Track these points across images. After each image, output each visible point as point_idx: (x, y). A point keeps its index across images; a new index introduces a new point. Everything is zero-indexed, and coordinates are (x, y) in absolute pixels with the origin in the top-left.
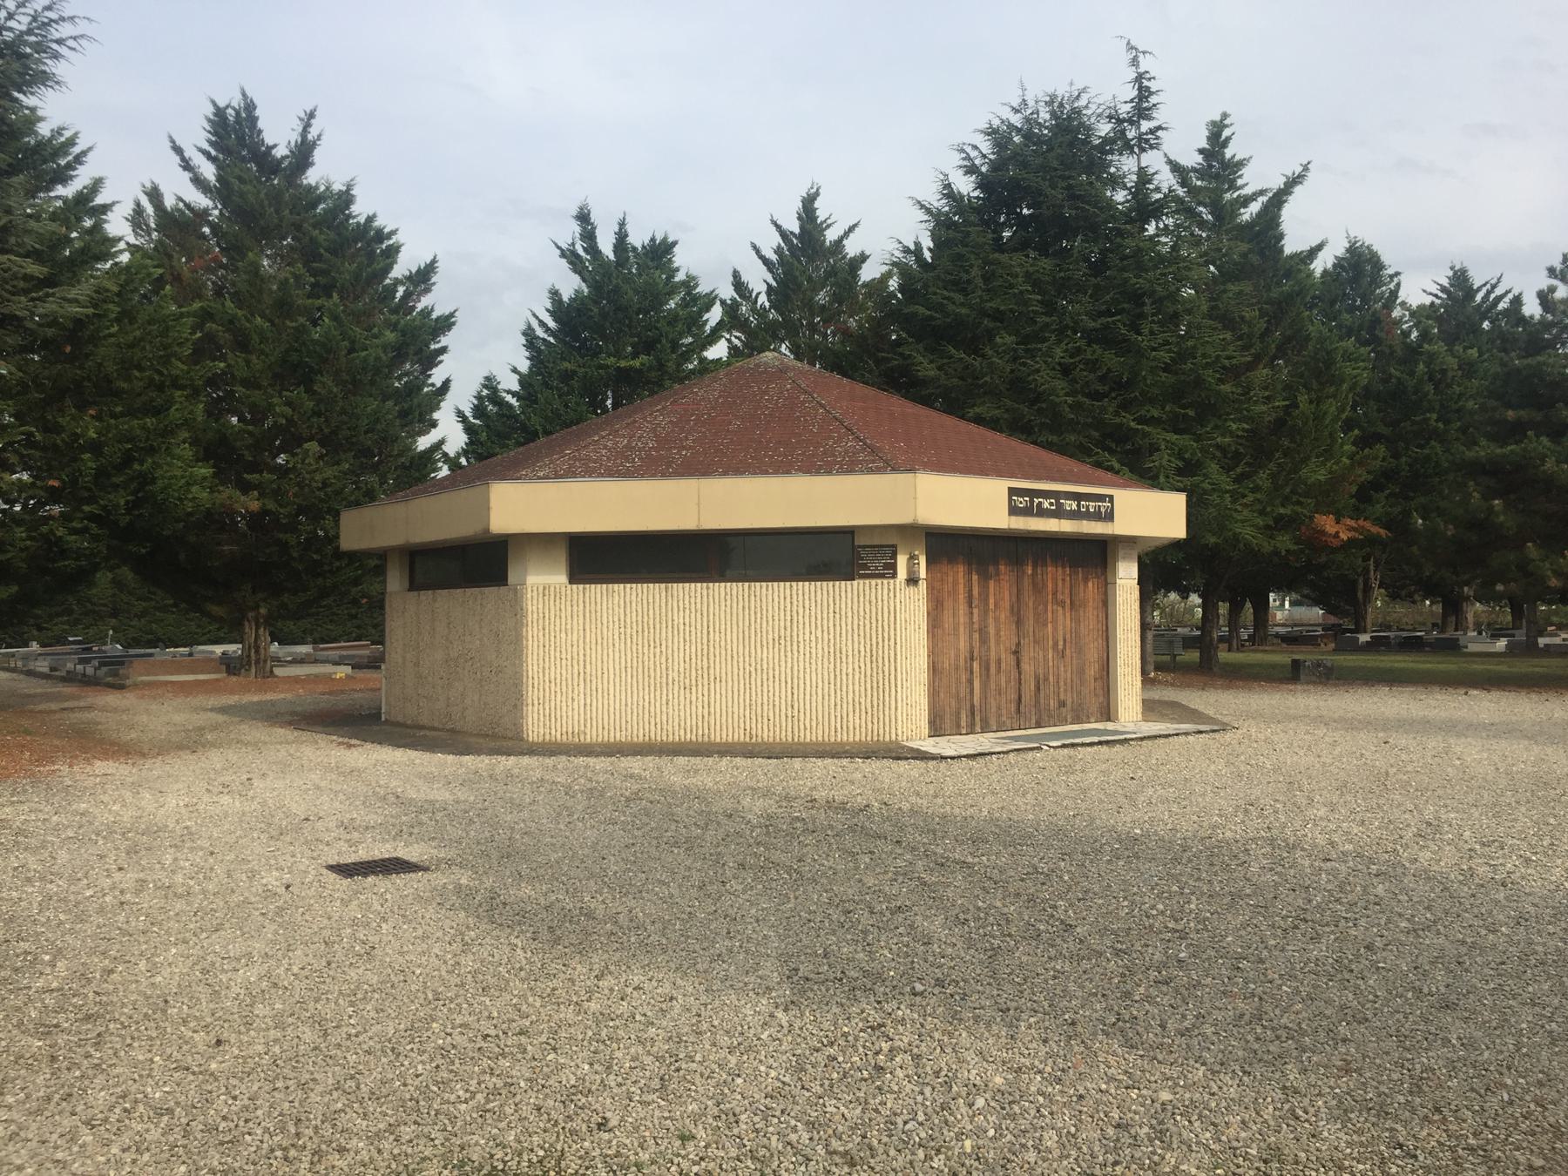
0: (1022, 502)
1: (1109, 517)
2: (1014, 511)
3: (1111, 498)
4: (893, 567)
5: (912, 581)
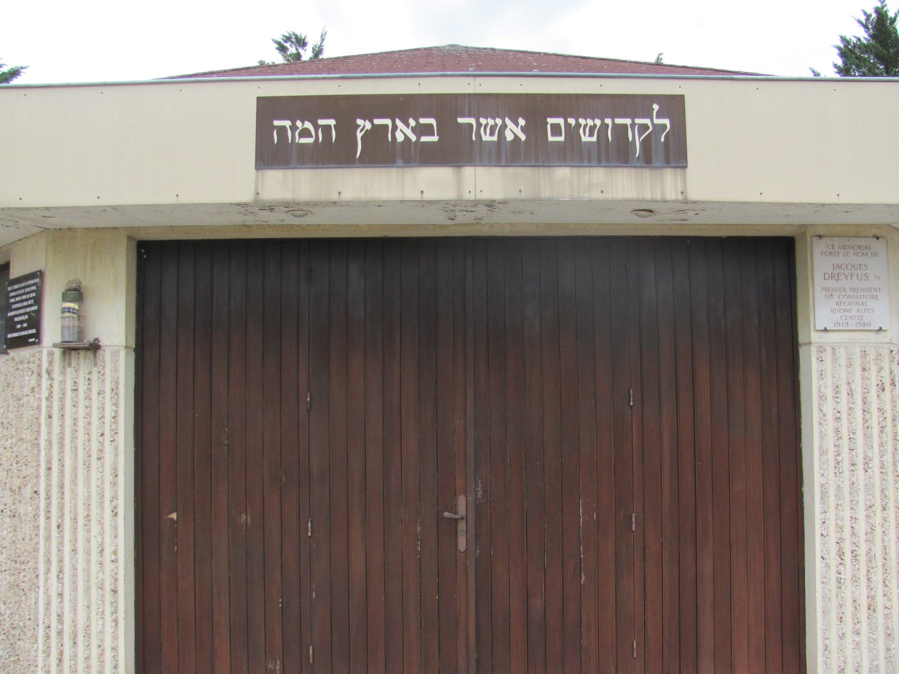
0: (305, 133)
1: (671, 151)
2: (272, 153)
4: (35, 321)
5: (81, 348)
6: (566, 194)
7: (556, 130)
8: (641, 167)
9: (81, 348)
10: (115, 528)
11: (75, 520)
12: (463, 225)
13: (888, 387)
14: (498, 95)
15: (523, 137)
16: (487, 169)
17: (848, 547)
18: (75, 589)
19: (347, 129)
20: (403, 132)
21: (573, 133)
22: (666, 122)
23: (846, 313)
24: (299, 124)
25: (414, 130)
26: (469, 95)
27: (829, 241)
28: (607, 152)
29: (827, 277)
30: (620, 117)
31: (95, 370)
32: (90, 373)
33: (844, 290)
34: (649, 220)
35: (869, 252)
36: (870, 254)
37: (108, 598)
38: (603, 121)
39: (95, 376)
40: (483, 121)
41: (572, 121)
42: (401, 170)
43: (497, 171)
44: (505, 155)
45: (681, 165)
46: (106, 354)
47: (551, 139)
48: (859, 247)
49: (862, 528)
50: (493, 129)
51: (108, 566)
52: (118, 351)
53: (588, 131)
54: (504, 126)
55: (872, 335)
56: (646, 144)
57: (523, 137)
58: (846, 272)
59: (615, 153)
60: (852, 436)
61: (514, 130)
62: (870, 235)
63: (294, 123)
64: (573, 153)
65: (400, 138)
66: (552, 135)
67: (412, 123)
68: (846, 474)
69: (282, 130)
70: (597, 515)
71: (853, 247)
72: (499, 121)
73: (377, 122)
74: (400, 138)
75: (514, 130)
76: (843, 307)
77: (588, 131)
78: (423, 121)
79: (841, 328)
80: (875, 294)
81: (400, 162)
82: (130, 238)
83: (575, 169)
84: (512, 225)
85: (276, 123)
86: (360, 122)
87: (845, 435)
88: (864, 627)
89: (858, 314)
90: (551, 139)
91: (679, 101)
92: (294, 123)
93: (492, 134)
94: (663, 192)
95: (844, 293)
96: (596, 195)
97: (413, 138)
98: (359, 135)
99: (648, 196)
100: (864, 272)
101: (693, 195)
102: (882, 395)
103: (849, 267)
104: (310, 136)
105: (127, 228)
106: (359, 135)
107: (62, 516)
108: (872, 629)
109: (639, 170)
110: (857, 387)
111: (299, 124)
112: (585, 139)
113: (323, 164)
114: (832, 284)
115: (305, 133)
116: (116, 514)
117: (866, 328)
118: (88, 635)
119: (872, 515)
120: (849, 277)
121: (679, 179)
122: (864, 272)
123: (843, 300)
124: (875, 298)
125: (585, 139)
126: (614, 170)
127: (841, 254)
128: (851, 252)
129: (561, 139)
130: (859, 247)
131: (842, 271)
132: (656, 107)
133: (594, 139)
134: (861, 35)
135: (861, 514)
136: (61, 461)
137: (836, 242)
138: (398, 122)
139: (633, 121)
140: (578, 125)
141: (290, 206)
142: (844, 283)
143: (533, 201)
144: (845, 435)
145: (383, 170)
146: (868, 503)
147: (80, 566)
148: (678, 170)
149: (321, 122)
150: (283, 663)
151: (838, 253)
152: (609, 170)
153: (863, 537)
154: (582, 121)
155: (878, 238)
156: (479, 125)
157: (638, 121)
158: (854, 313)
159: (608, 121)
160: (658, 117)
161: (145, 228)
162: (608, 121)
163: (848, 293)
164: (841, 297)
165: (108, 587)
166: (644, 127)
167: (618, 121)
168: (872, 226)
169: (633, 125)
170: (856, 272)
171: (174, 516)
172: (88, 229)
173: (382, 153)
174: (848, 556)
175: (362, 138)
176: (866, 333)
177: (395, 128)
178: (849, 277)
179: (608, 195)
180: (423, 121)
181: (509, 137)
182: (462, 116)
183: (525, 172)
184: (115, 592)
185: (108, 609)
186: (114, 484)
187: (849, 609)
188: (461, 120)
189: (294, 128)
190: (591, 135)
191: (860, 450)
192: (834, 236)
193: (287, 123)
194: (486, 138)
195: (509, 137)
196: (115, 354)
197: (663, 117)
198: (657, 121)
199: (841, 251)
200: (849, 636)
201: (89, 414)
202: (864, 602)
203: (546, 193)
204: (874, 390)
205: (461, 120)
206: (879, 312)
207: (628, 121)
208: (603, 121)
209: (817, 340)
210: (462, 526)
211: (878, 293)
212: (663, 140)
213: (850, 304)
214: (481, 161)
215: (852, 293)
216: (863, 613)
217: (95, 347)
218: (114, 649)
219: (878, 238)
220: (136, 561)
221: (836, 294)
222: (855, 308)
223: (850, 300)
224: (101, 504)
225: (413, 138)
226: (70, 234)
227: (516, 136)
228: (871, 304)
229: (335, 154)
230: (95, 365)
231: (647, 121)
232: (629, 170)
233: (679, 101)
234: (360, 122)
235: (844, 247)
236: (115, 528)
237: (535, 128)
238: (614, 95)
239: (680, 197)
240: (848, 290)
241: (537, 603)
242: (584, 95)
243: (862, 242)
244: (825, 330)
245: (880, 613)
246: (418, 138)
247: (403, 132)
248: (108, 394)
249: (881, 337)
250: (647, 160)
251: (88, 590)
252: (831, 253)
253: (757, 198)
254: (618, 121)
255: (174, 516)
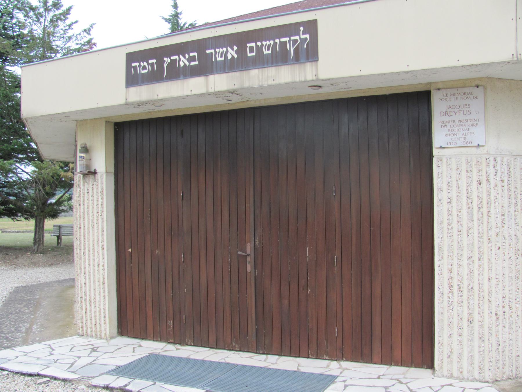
0: (143, 68)
1: (310, 53)
2: (133, 80)
3: (311, 26)
6: (255, 83)
7: (251, 49)
8: (294, 64)
9: (91, 173)
10: (103, 255)
11: (89, 251)
12: (236, 103)
13: (484, 182)
14: (224, 36)
15: (236, 56)
16: (220, 75)
17: (455, 283)
18: (90, 282)
19: (160, 63)
20: (183, 61)
21: (259, 50)
22: (307, 36)
23: (455, 136)
24: (142, 64)
25: (188, 60)
26: (212, 38)
27: (444, 92)
28: (276, 57)
29: (442, 114)
30: (283, 37)
31: (95, 183)
32: (93, 185)
33: (454, 121)
34: (320, 91)
35: (472, 96)
36: (472, 97)
37: (102, 286)
38: (274, 41)
39: (95, 186)
40: (217, 50)
41: (259, 44)
42: (182, 81)
43: (224, 76)
44: (229, 66)
45: (315, 59)
46: (98, 176)
47: (249, 55)
48: (465, 94)
49: (465, 271)
50: (222, 54)
51: (101, 272)
52: (103, 174)
53: (267, 47)
54: (227, 51)
55: (474, 149)
56: (296, 51)
57: (236, 56)
58: (456, 110)
59: (280, 58)
60: (459, 213)
61: (232, 53)
62: (474, 85)
63: (140, 64)
64: (261, 61)
65: (182, 64)
66: (250, 53)
67: (187, 56)
68: (455, 237)
69: (135, 67)
70: (316, 256)
71: (460, 94)
72: (225, 49)
73: (173, 58)
74: (182, 64)
75: (232, 53)
76: (454, 133)
77: (267, 47)
78: (191, 54)
79: (451, 146)
80: (475, 123)
81: (182, 77)
82: (107, 122)
83: (261, 70)
84: (265, 100)
85: (133, 65)
86: (165, 59)
87: (455, 212)
88: (465, 332)
89: (463, 136)
90: (249, 55)
91: (314, 23)
92: (140, 64)
93: (221, 57)
94: (305, 77)
95: (454, 124)
96: (271, 82)
97: (187, 64)
98: (165, 65)
99: (297, 80)
100: (467, 109)
101: (322, 76)
102: (480, 188)
103: (458, 107)
104: (146, 69)
105: (105, 118)
106: (165, 65)
107: (85, 249)
108: (471, 333)
109: (293, 66)
110: (464, 183)
111: (142, 64)
112: (266, 52)
113: (151, 82)
114: (446, 118)
115: (144, 68)
116: (103, 249)
117: (469, 145)
118: (95, 302)
119: (471, 263)
120: (457, 113)
121: (314, 68)
122: (467, 109)
123: (453, 128)
124: (476, 125)
125: (266, 52)
126: (280, 67)
127: (452, 99)
128: (459, 97)
129: (254, 54)
130: (465, 94)
131: (453, 110)
132: (302, 29)
133: (270, 52)
134: (68, 16)
135: (465, 262)
136: (84, 224)
137: (449, 92)
138: (181, 57)
139: (290, 39)
140: (262, 45)
141: (140, 104)
142: (454, 117)
143: (241, 89)
144: (455, 212)
145: (175, 82)
146: (469, 256)
147: (92, 271)
148: (314, 63)
149: (150, 61)
150: (173, 322)
151: (450, 98)
152: (277, 68)
153: (465, 277)
154: (264, 43)
155: (478, 87)
156: (216, 52)
157: (292, 38)
158: (461, 136)
159: (277, 41)
160: (303, 34)
161: (112, 117)
162: (277, 41)
163: (457, 123)
164: (452, 126)
165: (101, 281)
166: (296, 41)
167: (282, 40)
168: (475, 79)
169: (290, 41)
170: (462, 109)
171: (130, 250)
172: (91, 119)
173: (176, 73)
174: (455, 288)
175: (294, 50)
176: (470, 148)
177: (180, 59)
178: (457, 113)
179: (277, 82)
180: (191, 54)
181: (229, 57)
182: (209, 49)
183: (236, 75)
184: (104, 284)
185: (102, 291)
186: (102, 235)
187: (455, 320)
188: (208, 52)
189: (140, 66)
190: (268, 50)
191: (465, 222)
192: (447, 88)
193: (137, 64)
194: (219, 59)
195: (229, 57)
196: (102, 176)
197: (306, 34)
198: (302, 37)
199: (452, 97)
200: (455, 337)
201: (93, 204)
202: (465, 317)
203: (246, 85)
204: (475, 184)
205: (208, 52)
206: (477, 134)
207: (287, 39)
208: (274, 41)
209: (437, 154)
210: (249, 259)
211: (477, 122)
212: (305, 47)
213: (458, 130)
214: (217, 71)
215: (460, 123)
216: (465, 323)
217: (95, 173)
218: (104, 309)
219: (478, 87)
220: (117, 270)
221: (448, 125)
222: (461, 133)
223: (458, 128)
224: (98, 243)
225: (187, 64)
226: (83, 121)
227: (233, 56)
228: (473, 129)
229: (155, 77)
230: (95, 181)
231: (297, 38)
232: (287, 66)
233: (314, 23)
234: (165, 59)
235: (454, 94)
236: (103, 255)
237: (242, 51)
238: (280, 26)
239: (314, 78)
240: (457, 122)
241: (286, 302)
242: (265, 28)
243: (467, 90)
244: (441, 147)
245: (476, 324)
246: (190, 64)
247: (183, 61)
248: (100, 194)
249: (480, 150)
250: (297, 59)
251: (94, 282)
252: (445, 99)
253: (358, 73)
254: (282, 40)
255: (130, 250)
